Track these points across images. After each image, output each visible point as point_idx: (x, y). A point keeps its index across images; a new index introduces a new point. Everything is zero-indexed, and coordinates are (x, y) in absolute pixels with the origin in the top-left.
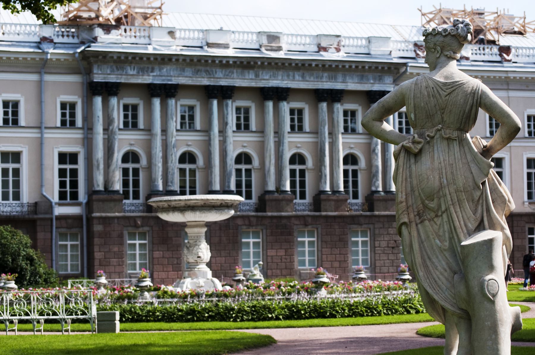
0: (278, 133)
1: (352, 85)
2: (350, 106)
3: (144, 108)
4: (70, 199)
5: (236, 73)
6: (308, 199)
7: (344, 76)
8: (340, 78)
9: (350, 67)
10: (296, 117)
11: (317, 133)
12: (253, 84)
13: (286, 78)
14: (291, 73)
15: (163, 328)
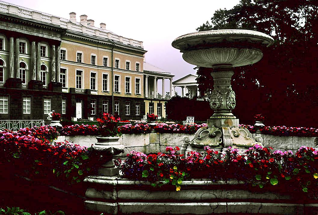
0: (15, 53)
2: (23, 41)
3: (27, 44)
4: (3, 81)
14: (21, 26)
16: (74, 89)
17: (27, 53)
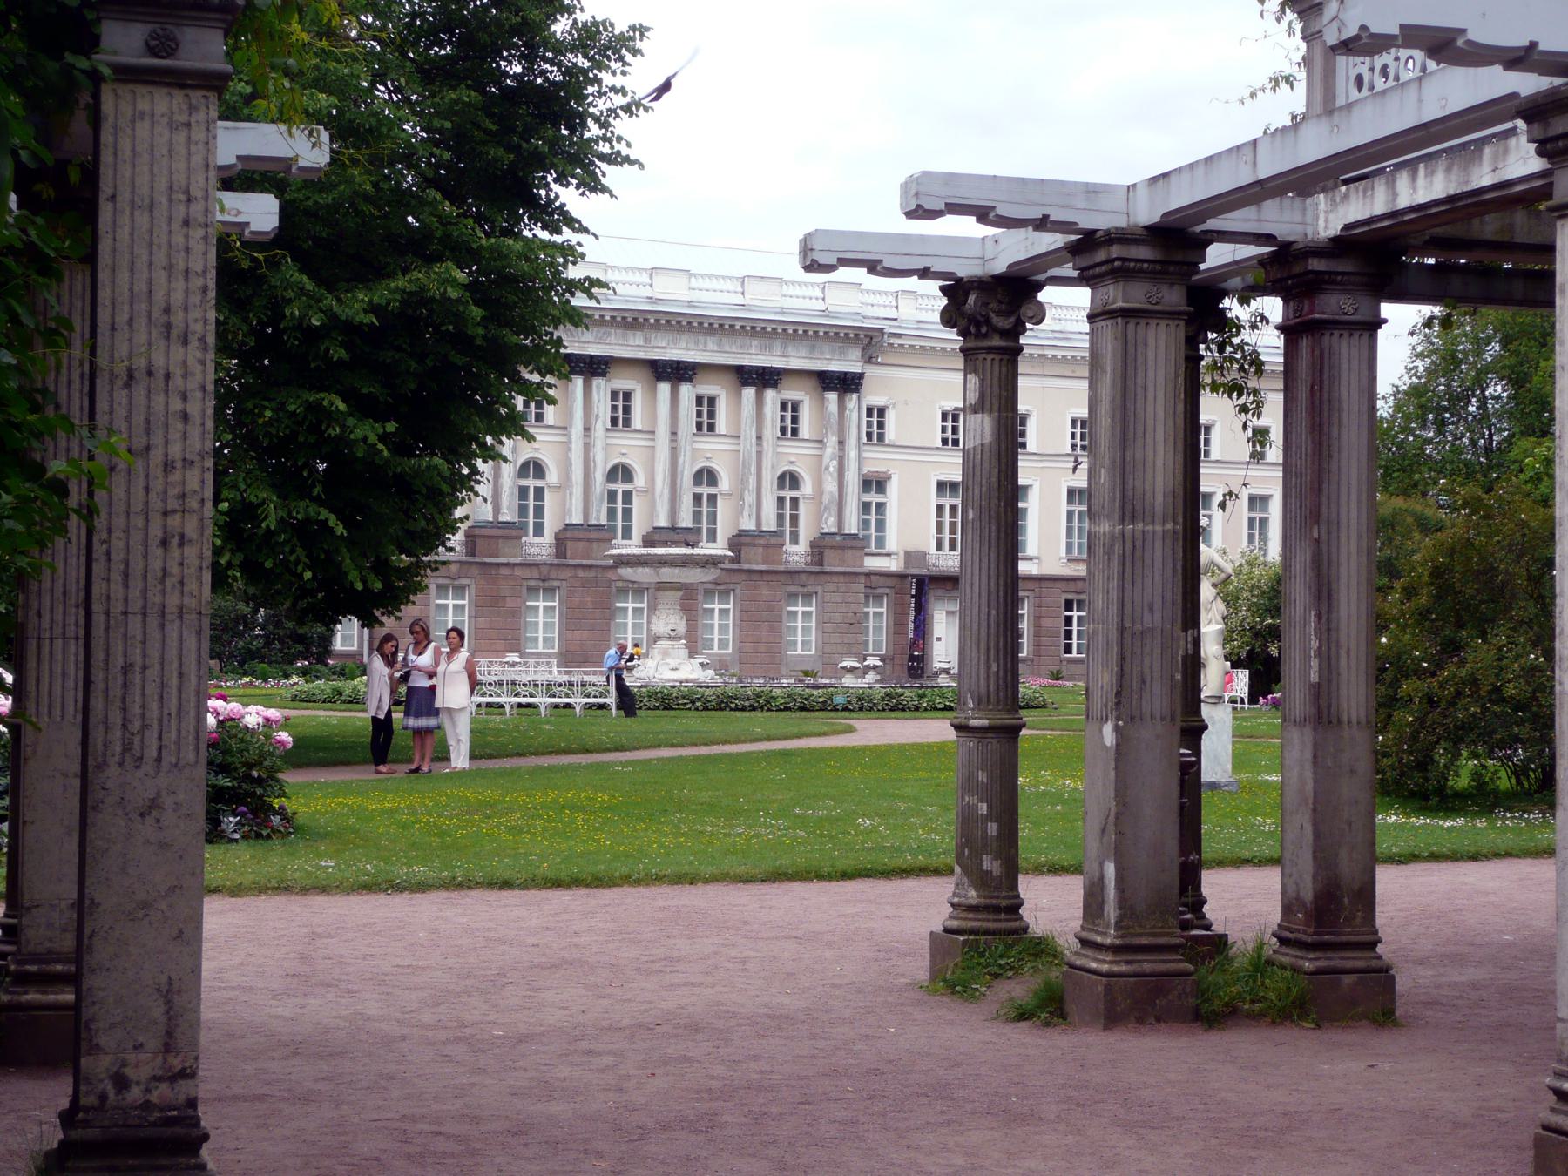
1: (797, 359)
5: (614, 335)
6: (548, 536)
7: (785, 347)
8: (778, 350)
9: (816, 332)
10: (620, 404)
11: (821, 441)
12: (641, 355)
13: (692, 346)
14: (701, 339)
15: (590, 742)
16: (925, 554)
17: (551, 423)
